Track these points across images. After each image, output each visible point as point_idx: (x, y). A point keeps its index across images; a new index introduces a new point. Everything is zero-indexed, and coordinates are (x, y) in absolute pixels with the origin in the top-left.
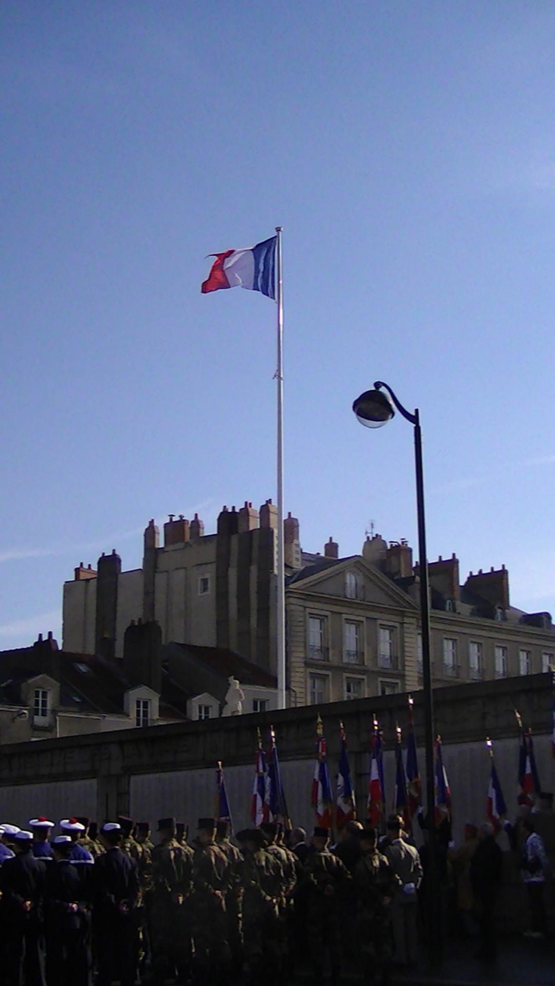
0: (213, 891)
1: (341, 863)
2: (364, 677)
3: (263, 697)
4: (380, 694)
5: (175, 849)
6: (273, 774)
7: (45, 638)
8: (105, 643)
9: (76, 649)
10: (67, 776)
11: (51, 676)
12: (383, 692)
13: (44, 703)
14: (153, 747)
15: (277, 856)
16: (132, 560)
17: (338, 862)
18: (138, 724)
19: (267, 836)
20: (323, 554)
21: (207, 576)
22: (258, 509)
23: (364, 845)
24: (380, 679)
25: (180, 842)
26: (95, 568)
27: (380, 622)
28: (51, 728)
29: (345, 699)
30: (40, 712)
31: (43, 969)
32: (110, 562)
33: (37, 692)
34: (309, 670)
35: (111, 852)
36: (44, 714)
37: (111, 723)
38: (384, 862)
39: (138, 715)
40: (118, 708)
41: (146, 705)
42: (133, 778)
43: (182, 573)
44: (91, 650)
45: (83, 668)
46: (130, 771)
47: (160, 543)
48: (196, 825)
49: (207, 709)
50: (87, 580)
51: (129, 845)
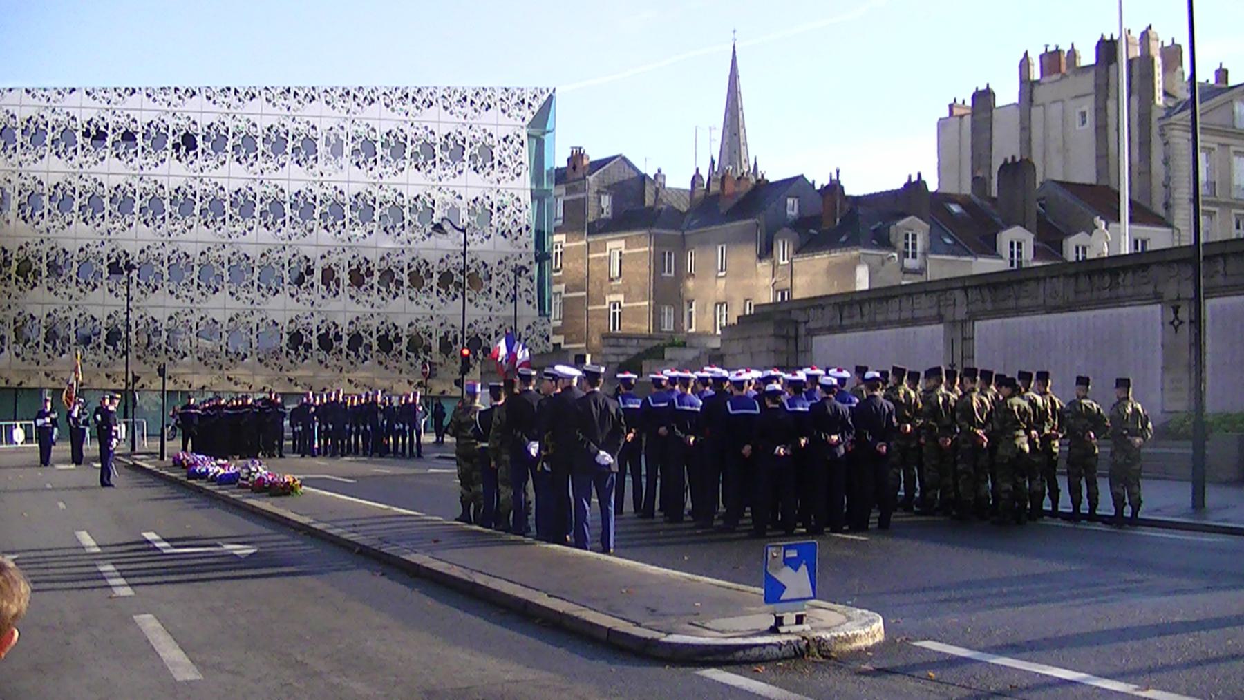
3: (1143, 236)
5: (943, 395)
7: (914, 178)
8: (979, 182)
9: (951, 189)
10: (915, 322)
13: (914, 246)
14: (1001, 293)
15: (1033, 403)
16: (1007, 94)
18: (1012, 264)
20: (1212, 81)
21: (1085, 108)
22: (1138, 36)
26: (969, 103)
27: (1232, 148)
28: (920, 271)
29: (1234, 237)
32: (983, 98)
33: (907, 235)
36: (914, 256)
38: (1138, 410)
41: (1019, 245)
42: (976, 323)
43: (1058, 107)
44: (967, 189)
45: (955, 208)
46: (973, 317)
47: (1036, 74)
49: (1084, 249)
50: (962, 116)
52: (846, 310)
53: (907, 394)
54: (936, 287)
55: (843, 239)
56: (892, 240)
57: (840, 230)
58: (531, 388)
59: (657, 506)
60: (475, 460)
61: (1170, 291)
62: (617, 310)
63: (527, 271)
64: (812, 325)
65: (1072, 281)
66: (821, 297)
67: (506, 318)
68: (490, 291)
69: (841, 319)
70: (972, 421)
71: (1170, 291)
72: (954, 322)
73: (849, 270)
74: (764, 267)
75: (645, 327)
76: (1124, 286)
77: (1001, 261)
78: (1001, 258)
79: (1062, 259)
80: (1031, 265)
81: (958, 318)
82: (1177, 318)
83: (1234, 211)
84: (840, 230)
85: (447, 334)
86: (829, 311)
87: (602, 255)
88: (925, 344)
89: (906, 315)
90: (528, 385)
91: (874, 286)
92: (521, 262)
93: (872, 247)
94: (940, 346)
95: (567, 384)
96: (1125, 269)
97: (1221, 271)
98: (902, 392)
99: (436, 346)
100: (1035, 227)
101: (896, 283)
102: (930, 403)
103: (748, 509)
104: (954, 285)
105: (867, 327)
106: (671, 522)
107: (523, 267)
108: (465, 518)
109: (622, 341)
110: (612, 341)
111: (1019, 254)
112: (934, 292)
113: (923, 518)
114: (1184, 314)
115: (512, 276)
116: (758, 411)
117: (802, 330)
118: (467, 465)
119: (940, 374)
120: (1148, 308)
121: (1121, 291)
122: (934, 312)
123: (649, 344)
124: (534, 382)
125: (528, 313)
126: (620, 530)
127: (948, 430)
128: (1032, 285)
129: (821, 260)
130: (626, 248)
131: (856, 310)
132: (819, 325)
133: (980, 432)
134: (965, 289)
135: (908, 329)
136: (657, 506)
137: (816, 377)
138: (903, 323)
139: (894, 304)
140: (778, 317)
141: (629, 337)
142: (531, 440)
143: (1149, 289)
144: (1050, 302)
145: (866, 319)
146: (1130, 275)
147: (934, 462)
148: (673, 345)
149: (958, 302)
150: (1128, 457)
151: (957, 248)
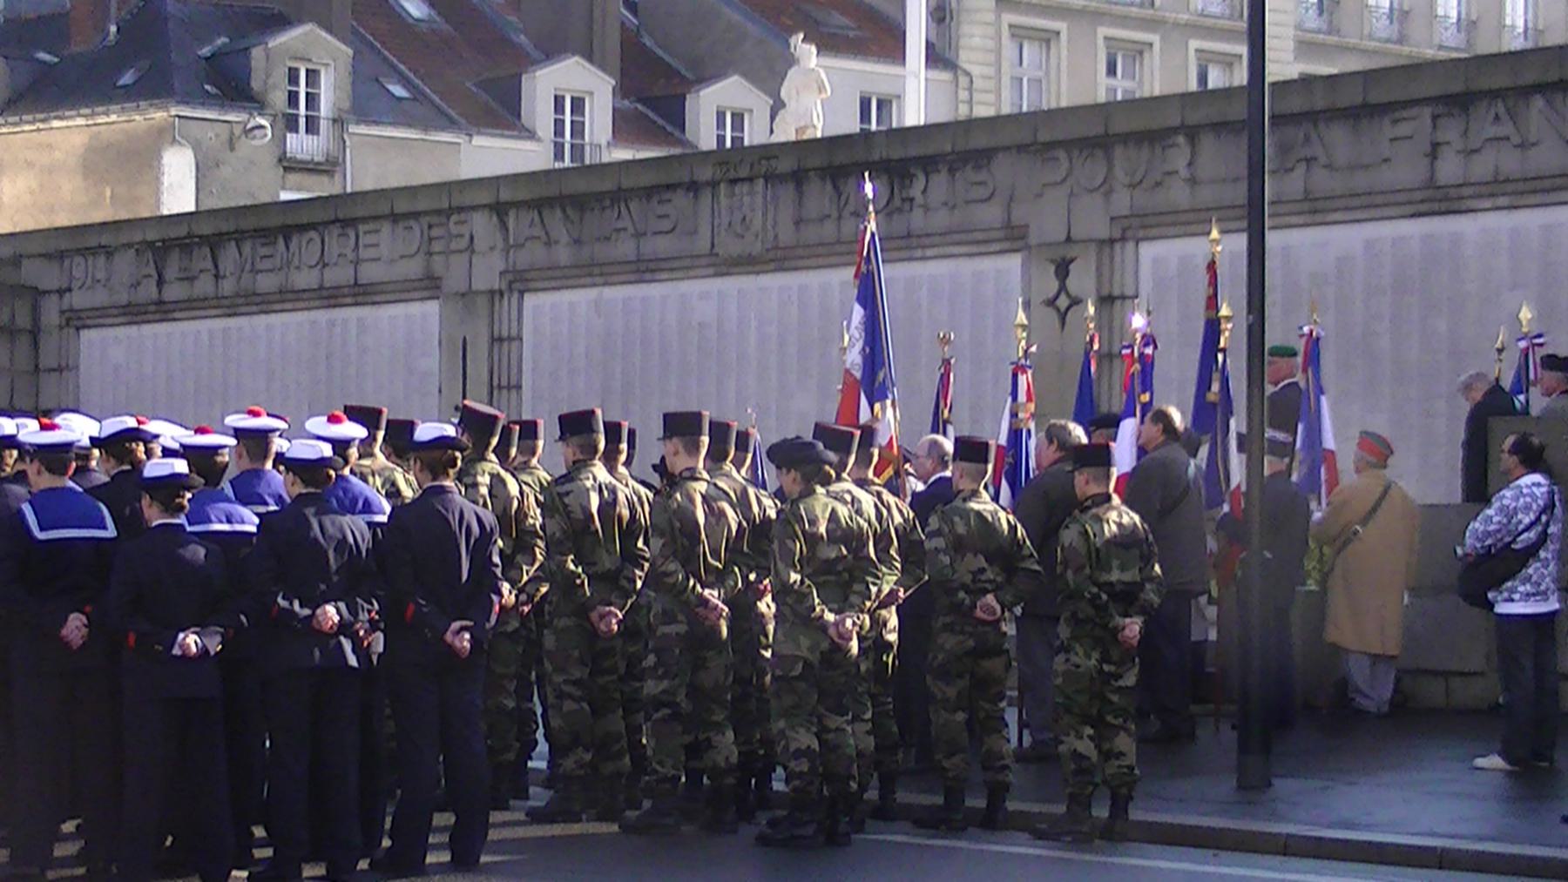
1: (1020, 531)
2: (1155, 38)
3: (884, 89)
4: (1193, 86)
6: (868, 294)
10: (362, 293)
11: (330, 31)
12: (1203, 78)
13: (312, 100)
14: (575, 216)
17: (1013, 529)
18: (559, 155)
19: (832, 456)
23: (1084, 484)
24: (1194, 44)
25: (612, 470)
28: (327, 167)
29: (1102, 97)
30: (302, 121)
33: (293, 77)
34: (1009, 18)
35: (432, 495)
36: (312, 126)
37: (488, 155)
39: (559, 132)
40: (502, 111)
41: (578, 105)
42: (530, 300)
46: (519, 282)
48: (659, 431)
49: (738, 118)
51: (486, 479)
52: (187, 264)
53: (497, 482)
55: (127, 78)
56: (256, 84)
57: (120, 56)
61: (1047, 222)
64: (78, 300)
65: (787, 192)
69: (161, 282)
70: (689, 559)
71: (1047, 222)
72: (467, 295)
73: (140, 160)
76: (926, 208)
77: (528, 145)
78: (531, 135)
79: (683, 143)
80: (606, 159)
81: (480, 284)
82: (1063, 288)
83: (1103, 31)
84: (120, 56)
86: (125, 264)
89: (339, 275)
91: (211, 203)
93: (206, 100)
96: (929, 164)
97: (1184, 173)
98: (484, 480)
100: (615, 61)
102: (567, 512)
103: (443, 819)
104: (468, 199)
105: (232, 306)
111: (578, 129)
112: (416, 215)
113: (557, 830)
114: (1082, 280)
116: (111, 532)
117: (51, 313)
119: (592, 430)
120: (987, 264)
121: (917, 220)
122: (413, 268)
127: (612, 583)
128: (680, 200)
129: (70, 133)
131: (202, 258)
132: (100, 298)
133: (712, 595)
134: (499, 210)
137: (263, 435)
138: (330, 297)
139: (307, 247)
143: (991, 214)
144: (730, 247)
145: (227, 287)
146: (940, 180)
147: (577, 673)
150: (1104, 659)
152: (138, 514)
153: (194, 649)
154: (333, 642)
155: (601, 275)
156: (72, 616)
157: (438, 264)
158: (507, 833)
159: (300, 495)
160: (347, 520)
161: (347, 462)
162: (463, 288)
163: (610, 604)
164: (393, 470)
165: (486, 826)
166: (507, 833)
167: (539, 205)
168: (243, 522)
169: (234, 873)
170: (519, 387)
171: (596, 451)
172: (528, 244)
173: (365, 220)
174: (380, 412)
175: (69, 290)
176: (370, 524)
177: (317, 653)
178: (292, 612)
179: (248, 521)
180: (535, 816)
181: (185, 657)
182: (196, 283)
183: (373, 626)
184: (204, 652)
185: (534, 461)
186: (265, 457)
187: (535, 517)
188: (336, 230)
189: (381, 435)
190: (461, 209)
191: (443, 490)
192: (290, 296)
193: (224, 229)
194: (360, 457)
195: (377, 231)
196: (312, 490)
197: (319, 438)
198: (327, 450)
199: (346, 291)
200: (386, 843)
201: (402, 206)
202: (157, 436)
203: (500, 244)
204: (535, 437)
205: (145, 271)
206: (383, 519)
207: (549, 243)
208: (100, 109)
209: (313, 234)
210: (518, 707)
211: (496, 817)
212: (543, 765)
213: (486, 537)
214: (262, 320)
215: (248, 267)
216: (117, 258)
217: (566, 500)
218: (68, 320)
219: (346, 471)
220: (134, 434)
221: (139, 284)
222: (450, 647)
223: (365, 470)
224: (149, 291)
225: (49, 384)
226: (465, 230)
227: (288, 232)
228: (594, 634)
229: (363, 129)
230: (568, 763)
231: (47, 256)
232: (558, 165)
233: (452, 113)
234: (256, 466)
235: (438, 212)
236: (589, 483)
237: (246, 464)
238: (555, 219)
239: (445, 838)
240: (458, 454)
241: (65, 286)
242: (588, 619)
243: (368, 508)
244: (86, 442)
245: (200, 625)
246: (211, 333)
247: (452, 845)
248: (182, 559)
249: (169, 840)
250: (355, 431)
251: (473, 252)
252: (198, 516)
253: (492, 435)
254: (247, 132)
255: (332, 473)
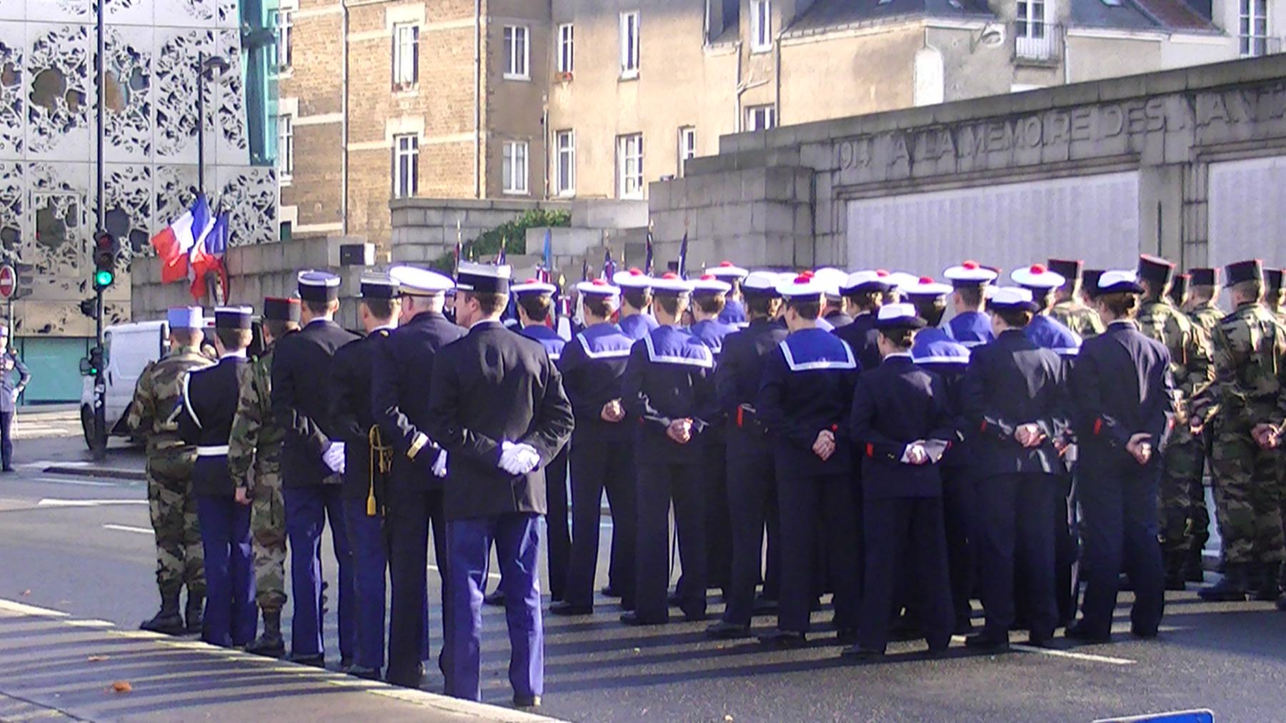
0: (1007, 429)
10: (1075, 167)
28: (1051, 63)
30: (1029, 27)
31: (388, 605)
36: (1038, 30)
37: (1185, 49)
39: (1246, 28)
42: (1216, 170)
46: (1206, 154)
52: (930, 145)
54: (1125, 92)
58: (328, 317)
59: (602, 579)
60: (189, 487)
62: (410, 152)
63: (224, 68)
64: (846, 177)
66: (866, 117)
67: (179, 168)
68: (145, 109)
69: (912, 161)
72: (1163, 166)
73: (897, 62)
74: (723, 56)
75: (468, 188)
78: (1220, 31)
81: (1173, 157)
85: (51, 207)
86: (883, 149)
87: (375, 35)
88: (1107, 217)
89: (1056, 152)
90: (323, 310)
92: (210, 49)
94: (1132, 222)
95: (419, 307)
99: (28, 229)
101: (1000, 90)
102: (1230, 345)
103: (1126, 597)
105: (970, 179)
106: (640, 621)
107: (215, 60)
108: (165, 622)
109: (434, 217)
110: (413, 217)
111: (1262, 25)
115: (191, 78)
116: (851, 364)
117: (825, 187)
118: (170, 497)
119: (1254, 277)
122: (1118, 145)
123: (492, 221)
124: (334, 303)
125: (228, 157)
126: (557, 638)
129: (844, 42)
130: (428, 19)
132: (863, 175)
134: (1189, 94)
135: (1057, 184)
136: (602, 579)
138: (1048, 170)
139: (1029, 130)
140: (773, 161)
141: (447, 207)
142: (332, 439)
145: (966, 164)
147: (1239, 479)
148: (540, 223)
149: (1173, 124)
151: (1128, 14)
152: (874, 348)
153: (919, 458)
154: (1032, 454)
155: (1275, 147)
156: (822, 433)
157: (1138, 141)
158: (1182, 609)
159: (1004, 332)
160: (1042, 352)
161: (1044, 305)
162: (1160, 160)
163: (1269, 422)
164: (1087, 311)
165: (1162, 604)
166: (1182, 609)
167: (1221, 90)
168: (958, 355)
169: (954, 638)
170: (1206, 242)
171: (1257, 295)
172: (1213, 124)
173: (1077, 106)
174: (1075, 265)
175: (840, 169)
176: (1064, 357)
177: (1019, 463)
178: (998, 426)
179: (962, 354)
180: (1207, 596)
181: (912, 464)
182: (940, 162)
183: (1068, 440)
184: (928, 460)
185: (1211, 303)
186: (977, 303)
187: (1206, 348)
188: (1053, 116)
189: (1079, 283)
190: (1155, 96)
191: (1123, 326)
192: (1017, 170)
193: (963, 117)
194: (1060, 301)
195: (1087, 116)
196: (1013, 328)
197: (1024, 286)
198: (1027, 296)
199: (1061, 165)
200: (1079, 615)
201: (1108, 95)
202: (892, 287)
203: (1189, 124)
204: (1212, 282)
205: (899, 153)
206: (1075, 351)
207: (1232, 121)
208: (867, 23)
209: (1034, 119)
210: (1193, 506)
211: (1170, 595)
212: (1217, 553)
213: (1161, 364)
214: (993, 191)
215: (982, 147)
216: (877, 141)
217: (1230, 336)
218: (839, 194)
219: (1046, 313)
220: (873, 287)
221: (894, 163)
222: (1132, 455)
223: (1066, 312)
224: (902, 169)
225: (824, 245)
226: (1158, 112)
227: (1014, 118)
228: (1256, 448)
229: (1079, 32)
230: (1233, 553)
231: (822, 143)
232: (1244, 56)
233: (1154, 16)
234: (971, 309)
235: (1137, 98)
236: (1250, 322)
237: (963, 308)
238: (1237, 104)
239: (1127, 612)
240: (1135, 296)
241: (835, 165)
242: (1250, 435)
243: (1063, 342)
244: (837, 293)
245: (925, 436)
246: (952, 202)
247: (1134, 618)
248: (908, 385)
249: (903, 611)
250: (1056, 280)
251: (1166, 131)
252: (922, 351)
253: (1165, 282)
254: (985, 37)
255: (1030, 315)
